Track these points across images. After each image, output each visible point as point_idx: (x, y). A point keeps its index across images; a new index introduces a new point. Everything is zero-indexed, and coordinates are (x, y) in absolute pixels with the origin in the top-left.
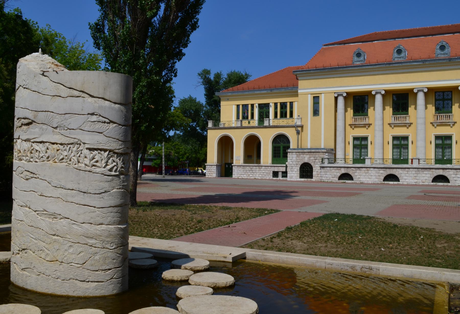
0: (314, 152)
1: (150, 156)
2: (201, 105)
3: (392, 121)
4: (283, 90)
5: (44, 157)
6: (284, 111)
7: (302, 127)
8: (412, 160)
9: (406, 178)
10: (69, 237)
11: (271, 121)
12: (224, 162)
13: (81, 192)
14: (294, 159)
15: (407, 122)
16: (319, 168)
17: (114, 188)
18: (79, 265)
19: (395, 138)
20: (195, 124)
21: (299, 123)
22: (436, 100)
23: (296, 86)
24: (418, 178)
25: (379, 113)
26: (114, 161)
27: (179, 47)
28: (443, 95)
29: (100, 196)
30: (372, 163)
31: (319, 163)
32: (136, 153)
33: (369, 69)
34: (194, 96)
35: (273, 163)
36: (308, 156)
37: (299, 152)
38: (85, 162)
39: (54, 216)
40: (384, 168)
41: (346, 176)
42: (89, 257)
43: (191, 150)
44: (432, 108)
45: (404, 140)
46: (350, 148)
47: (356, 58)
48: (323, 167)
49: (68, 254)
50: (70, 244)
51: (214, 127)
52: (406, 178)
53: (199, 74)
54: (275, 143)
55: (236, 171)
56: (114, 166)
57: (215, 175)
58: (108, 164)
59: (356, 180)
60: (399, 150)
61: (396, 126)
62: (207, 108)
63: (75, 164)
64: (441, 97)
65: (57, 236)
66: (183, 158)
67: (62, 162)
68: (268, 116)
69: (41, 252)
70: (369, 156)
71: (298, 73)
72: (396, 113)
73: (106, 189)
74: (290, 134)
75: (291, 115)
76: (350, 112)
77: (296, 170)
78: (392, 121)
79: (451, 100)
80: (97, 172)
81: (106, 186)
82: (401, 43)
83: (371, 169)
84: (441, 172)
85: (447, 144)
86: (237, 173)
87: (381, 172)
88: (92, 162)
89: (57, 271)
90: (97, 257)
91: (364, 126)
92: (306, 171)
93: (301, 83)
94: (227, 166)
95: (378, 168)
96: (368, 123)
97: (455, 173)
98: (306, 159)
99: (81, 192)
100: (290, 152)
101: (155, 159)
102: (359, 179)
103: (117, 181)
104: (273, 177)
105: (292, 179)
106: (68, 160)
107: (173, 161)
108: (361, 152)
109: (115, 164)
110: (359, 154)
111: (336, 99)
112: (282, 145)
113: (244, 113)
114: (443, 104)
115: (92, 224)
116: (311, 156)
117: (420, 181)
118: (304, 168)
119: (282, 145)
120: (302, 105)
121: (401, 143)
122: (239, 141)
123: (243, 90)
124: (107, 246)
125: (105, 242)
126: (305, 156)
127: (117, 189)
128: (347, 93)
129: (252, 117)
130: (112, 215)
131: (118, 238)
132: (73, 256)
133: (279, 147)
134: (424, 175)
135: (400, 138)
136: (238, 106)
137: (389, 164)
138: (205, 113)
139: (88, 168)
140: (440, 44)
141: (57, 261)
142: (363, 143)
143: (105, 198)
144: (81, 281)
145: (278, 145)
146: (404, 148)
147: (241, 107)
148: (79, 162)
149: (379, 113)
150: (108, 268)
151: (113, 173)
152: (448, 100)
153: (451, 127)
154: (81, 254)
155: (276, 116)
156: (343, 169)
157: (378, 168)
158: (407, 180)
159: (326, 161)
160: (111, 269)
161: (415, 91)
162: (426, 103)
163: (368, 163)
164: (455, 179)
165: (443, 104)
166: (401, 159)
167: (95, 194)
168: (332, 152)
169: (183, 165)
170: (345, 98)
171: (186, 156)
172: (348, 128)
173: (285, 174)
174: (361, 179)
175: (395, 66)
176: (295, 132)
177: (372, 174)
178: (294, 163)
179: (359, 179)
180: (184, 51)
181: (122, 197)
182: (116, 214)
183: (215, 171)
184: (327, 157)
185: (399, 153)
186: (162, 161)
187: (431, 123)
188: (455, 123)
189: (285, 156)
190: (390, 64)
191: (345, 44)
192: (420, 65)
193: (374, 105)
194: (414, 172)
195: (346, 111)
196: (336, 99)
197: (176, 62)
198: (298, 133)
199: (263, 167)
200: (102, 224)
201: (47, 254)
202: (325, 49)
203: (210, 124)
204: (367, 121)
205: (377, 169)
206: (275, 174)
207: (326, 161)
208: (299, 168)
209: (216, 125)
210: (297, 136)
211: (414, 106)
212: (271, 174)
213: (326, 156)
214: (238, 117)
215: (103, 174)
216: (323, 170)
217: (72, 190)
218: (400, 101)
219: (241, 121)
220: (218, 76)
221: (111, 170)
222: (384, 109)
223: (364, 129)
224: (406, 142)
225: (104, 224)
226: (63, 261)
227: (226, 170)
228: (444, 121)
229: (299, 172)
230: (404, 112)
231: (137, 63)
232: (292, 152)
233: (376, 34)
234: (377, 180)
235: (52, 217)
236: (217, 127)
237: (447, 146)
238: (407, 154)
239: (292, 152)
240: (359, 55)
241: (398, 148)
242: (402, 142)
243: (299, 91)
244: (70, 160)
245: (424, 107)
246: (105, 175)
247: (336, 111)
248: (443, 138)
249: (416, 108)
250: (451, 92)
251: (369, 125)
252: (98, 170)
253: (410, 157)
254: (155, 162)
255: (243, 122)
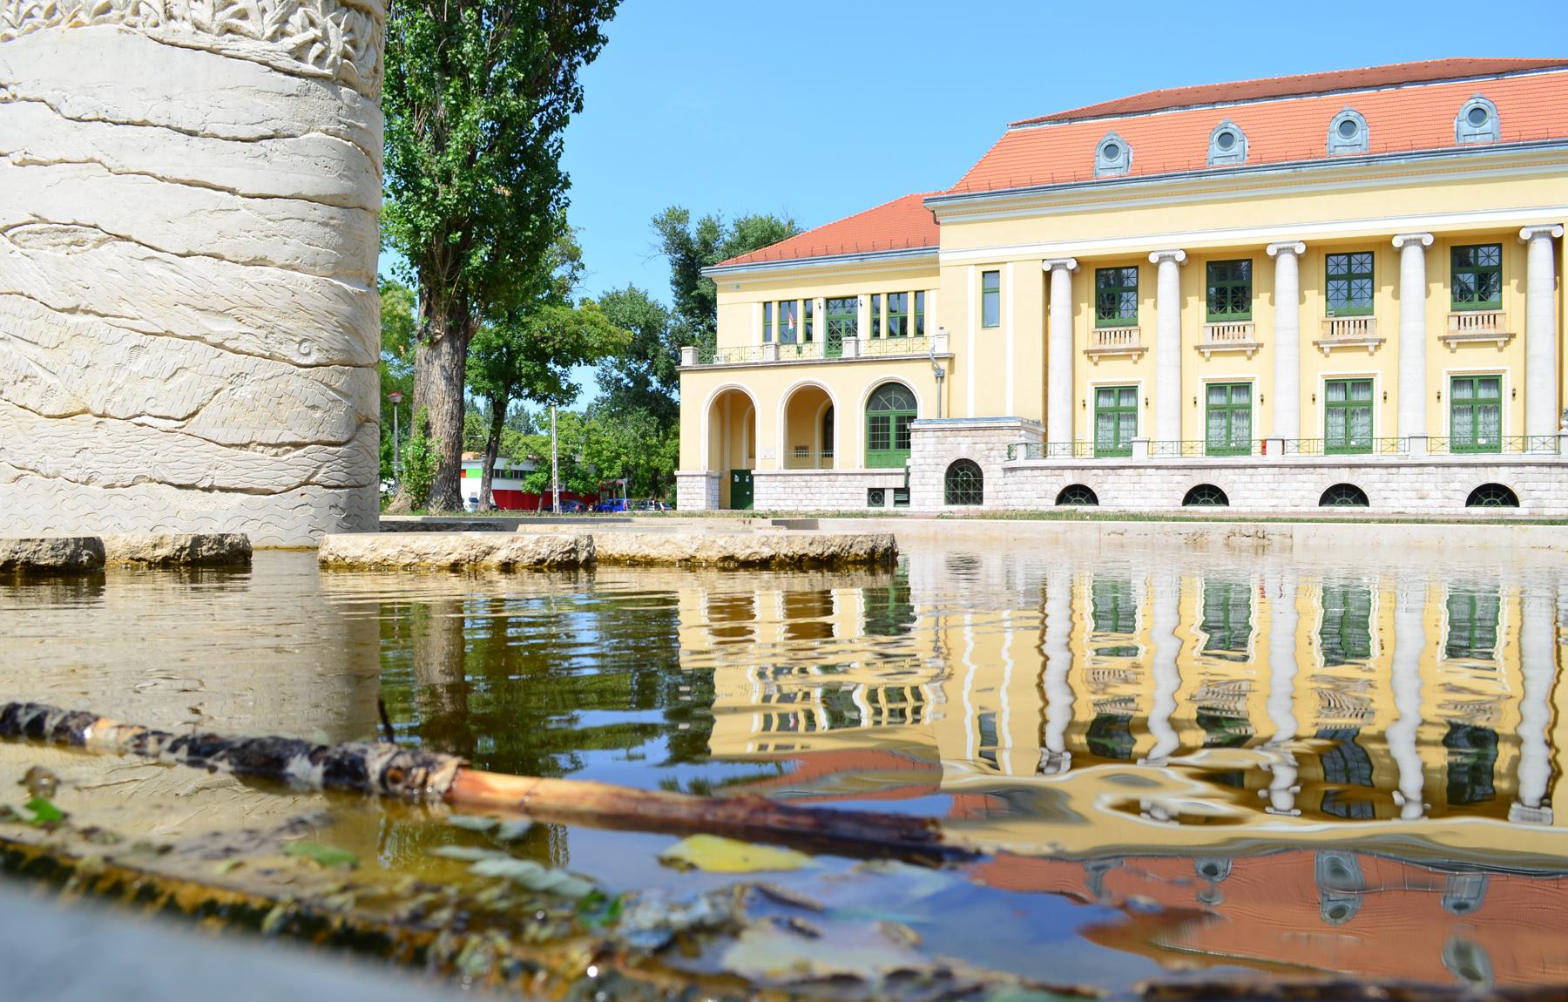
0: (985, 429)
1: (518, 463)
2: (661, 312)
3: (1205, 338)
4: (895, 258)
5: (35, 11)
6: (900, 321)
7: (951, 359)
8: (1264, 443)
9: (1247, 494)
10: (133, 314)
11: (861, 344)
12: (728, 469)
13: (179, 130)
14: (930, 448)
15: (1248, 340)
16: (1001, 474)
17: (311, 125)
18: (172, 424)
19: (1214, 388)
20: (645, 366)
21: (942, 349)
22: (1329, 278)
23: (931, 245)
24: (1279, 494)
25: (1170, 314)
26: (312, 23)
27: (586, 19)
28: (1349, 264)
29: (257, 148)
30: (1151, 454)
31: (1000, 460)
32: (458, 344)
33: (1089, 193)
34: (641, 287)
35: (867, 466)
36: (969, 440)
37: (942, 430)
38: (195, 14)
39: (72, 233)
40: (1185, 467)
41: (1078, 494)
42: (211, 388)
43: (635, 440)
44: (1316, 300)
45: (1239, 394)
46: (1087, 418)
47: (1103, 161)
48: (1012, 469)
49: (127, 381)
50: (136, 339)
51: (699, 366)
52: (1247, 494)
53: (655, 221)
54: (876, 408)
55: (763, 490)
56: (314, 41)
57: (703, 503)
58: (289, 28)
59: (1236, 505)
60: (1224, 422)
61: (1217, 352)
62: (676, 321)
63: (157, 25)
64: (1343, 270)
65: (87, 312)
66: (611, 468)
67: (104, 21)
68: (852, 331)
69: (27, 384)
70: (1142, 435)
71: (939, 203)
72: (1218, 315)
73: (279, 125)
74: (917, 378)
75: (920, 331)
76: (1088, 312)
77: (934, 481)
78: (1205, 338)
79: (1370, 276)
80: (242, 54)
81: (281, 112)
82: (1227, 116)
83: (1149, 471)
84: (1344, 477)
85: (1359, 403)
86: (765, 495)
87: (1178, 478)
88: (219, 15)
89: (87, 453)
90: (245, 392)
91: (1127, 354)
92: (964, 482)
93: (949, 234)
94: (737, 479)
95: (1167, 468)
96: (1137, 346)
97: (1385, 478)
98: (964, 449)
99: (179, 130)
100: (916, 430)
101: (531, 473)
102: (1116, 502)
103: (321, 103)
104: (870, 504)
105: (922, 509)
106: (129, 11)
107: (585, 478)
108: (1474, 423)
109: (319, 33)
110: (1111, 435)
111: (1048, 276)
112: (893, 413)
113: (783, 324)
114: (1349, 290)
115: (221, 258)
116: (978, 440)
117: (1287, 502)
118: (957, 475)
119: (893, 413)
120: (949, 299)
121: (1230, 400)
122: (771, 404)
123: (782, 260)
124: (284, 350)
125: (278, 335)
126: (960, 440)
127: (326, 132)
128: (1079, 262)
129: (809, 337)
130: (304, 234)
131: (330, 327)
132: (149, 388)
133: (887, 419)
134: (1296, 485)
135: (1476, 381)
136: (767, 305)
137: (1198, 456)
138: (673, 334)
139: (206, 40)
140: (1342, 118)
141: (85, 412)
142: (1124, 403)
143: (276, 158)
144: (180, 487)
145: (881, 413)
146: (1487, 411)
147: (775, 306)
148: (171, 17)
149: (1170, 314)
150: (289, 437)
151: (309, 67)
152: (1362, 276)
153: (1372, 354)
154: (178, 380)
155: (876, 334)
156: (1068, 473)
157: (1167, 468)
158: (1249, 502)
159: (1021, 452)
160: (303, 445)
161: (1153, 259)
162: (1429, 278)
163: (1140, 455)
164: (1384, 494)
165: (1349, 290)
166: (1228, 446)
167: (235, 139)
168: (1039, 431)
169: (613, 489)
170: (1073, 274)
171: (619, 463)
172: (1081, 359)
173: (903, 494)
174: (1121, 502)
175: (1213, 182)
176: (932, 374)
177: (1152, 486)
178: (929, 461)
179: (1116, 502)
180: (604, 27)
181: (348, 168)
182: (321, 230)
183: (704, 491)
184: (1023, 440)
185: (1224, 432)
186: (550, 478)
187: (1316, 343)
188: (1383, 341)
189: (904, 443)
190: (1200, 174)
191: (1071, 119)
192: (1285, 176)
193: (1154, 294)
194: (1269, 478)
195: (1075, 311)
196: (1048, 276)
197: (579, 63)
198: (940, 377)
199: (841, 478)
200: (260, 262)
201: (49, 389)
202: (1017, 135)
203: (688, 356)
204: (1135, 342)
205: (1165, 472)
206: (876, 495)
207: (1021, 452)
208: (943, 476)
209: (706, 358)
210: (936, 386)
211: (1268, 295)
212: (865, 497)
213: (1020, 438)
214: (767, 336)
215: (266, 64)
216: (1011, 477)
217: (143, 124)
218: (1229, 283)
219: (777, 346)
220: (710, 228)
221: (298, 53)
222: (1183, 304)
223: (1128, 363)
224: (1243, 399)
225: (272, 263)
226: (109, 411)
227: (737, 492)
228: (1351, 337)
229: (942, 487)
230: (1240, 314)
231: (455, 56)
232: (924, 431)
233: (1158, 94)
234: (1164, 502)
235: (67, 239)
236: (706, 366)
237: (1358, 409)
238: (1246, 432)
239: (924, 431)
240: (1111, 150)
241: (1222, 415)
242: (1235, 399)
243: (942, 257)
244: (137, 12)
245: (1296, 297)
246: (276, 69)
247: (1047, 312)
248: (1349, 384)
249: (1396, 295)
250: (1136, 268)
251: (1142, 351)
252: (245, 46)
253: (1257, 434)
254: (532, 478)
255: (783, 349)
